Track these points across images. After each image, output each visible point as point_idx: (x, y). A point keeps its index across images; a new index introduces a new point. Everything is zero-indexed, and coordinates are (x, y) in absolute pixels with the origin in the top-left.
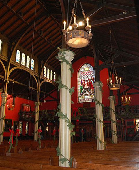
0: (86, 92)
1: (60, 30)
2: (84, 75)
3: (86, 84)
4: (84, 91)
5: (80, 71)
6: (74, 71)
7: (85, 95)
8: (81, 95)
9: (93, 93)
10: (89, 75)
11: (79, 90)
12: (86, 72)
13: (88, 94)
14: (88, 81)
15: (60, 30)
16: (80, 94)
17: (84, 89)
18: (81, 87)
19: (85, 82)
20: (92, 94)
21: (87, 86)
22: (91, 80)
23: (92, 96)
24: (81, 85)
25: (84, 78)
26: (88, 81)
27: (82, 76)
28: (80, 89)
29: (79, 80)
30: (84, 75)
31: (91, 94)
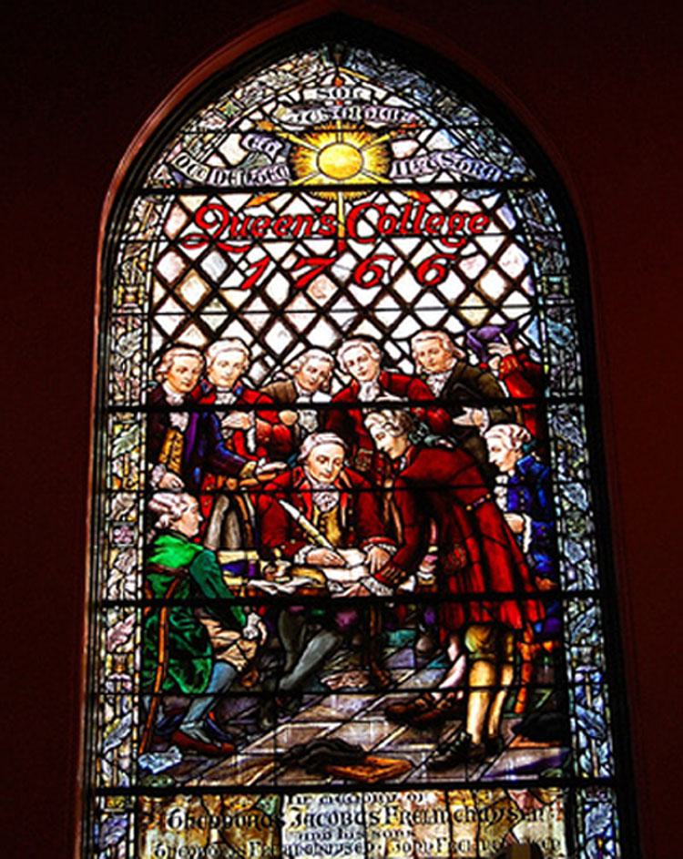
0: (312, 689)
1: (161, 733)
2: (278, 289)
3: (326, 501)
4: (271, 654)
5: (161, 173)
6: (180, 756)
7: (297, 758)
8: (159, 763)
9: (534, 728)
10: (407, 287)
11: (121, 631)
12: (339, 209)
13: (364, 734)
14: (384, 433)
15: (161, 733)
16: (154, 735)
17: (270, 606)
18: (173, 556)
19: (286, 446)
20: (493, 745)
21: (355, 537)
22: (473, 416)
23: (504, 815)
24: (182, 510)
25: (278, 339)
26: (384, 433)
27: (215, 290)
28: (148, 602)
29: (127, 380)
30: (278, 289)
31: (464, 755)
